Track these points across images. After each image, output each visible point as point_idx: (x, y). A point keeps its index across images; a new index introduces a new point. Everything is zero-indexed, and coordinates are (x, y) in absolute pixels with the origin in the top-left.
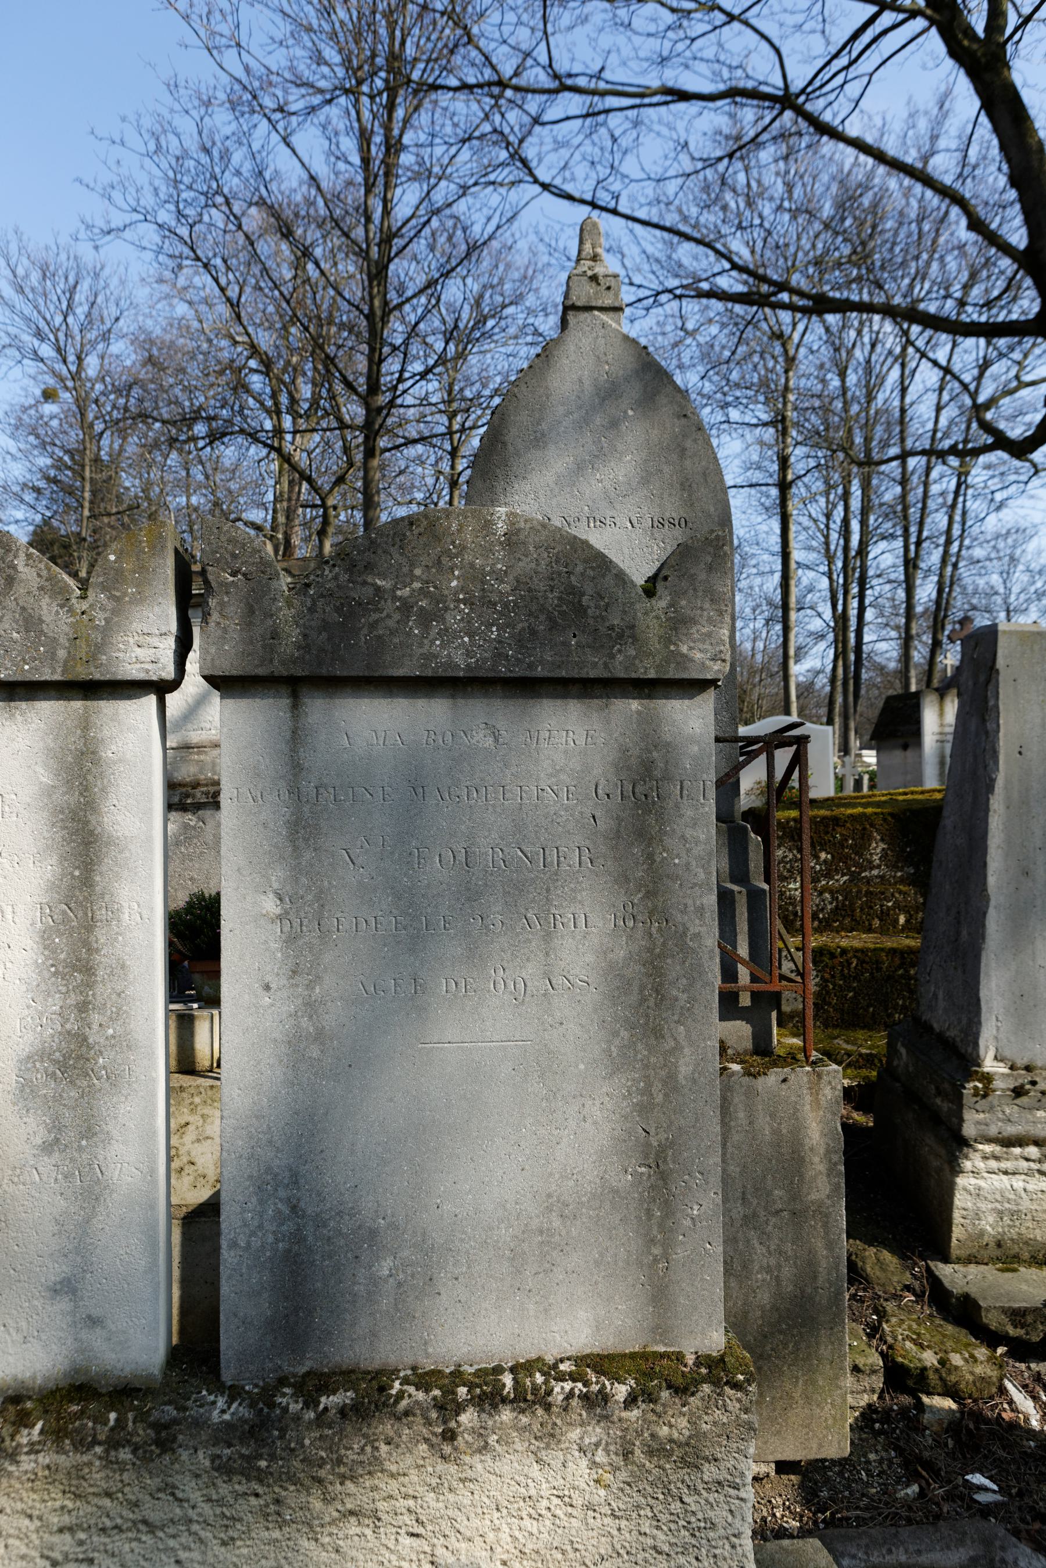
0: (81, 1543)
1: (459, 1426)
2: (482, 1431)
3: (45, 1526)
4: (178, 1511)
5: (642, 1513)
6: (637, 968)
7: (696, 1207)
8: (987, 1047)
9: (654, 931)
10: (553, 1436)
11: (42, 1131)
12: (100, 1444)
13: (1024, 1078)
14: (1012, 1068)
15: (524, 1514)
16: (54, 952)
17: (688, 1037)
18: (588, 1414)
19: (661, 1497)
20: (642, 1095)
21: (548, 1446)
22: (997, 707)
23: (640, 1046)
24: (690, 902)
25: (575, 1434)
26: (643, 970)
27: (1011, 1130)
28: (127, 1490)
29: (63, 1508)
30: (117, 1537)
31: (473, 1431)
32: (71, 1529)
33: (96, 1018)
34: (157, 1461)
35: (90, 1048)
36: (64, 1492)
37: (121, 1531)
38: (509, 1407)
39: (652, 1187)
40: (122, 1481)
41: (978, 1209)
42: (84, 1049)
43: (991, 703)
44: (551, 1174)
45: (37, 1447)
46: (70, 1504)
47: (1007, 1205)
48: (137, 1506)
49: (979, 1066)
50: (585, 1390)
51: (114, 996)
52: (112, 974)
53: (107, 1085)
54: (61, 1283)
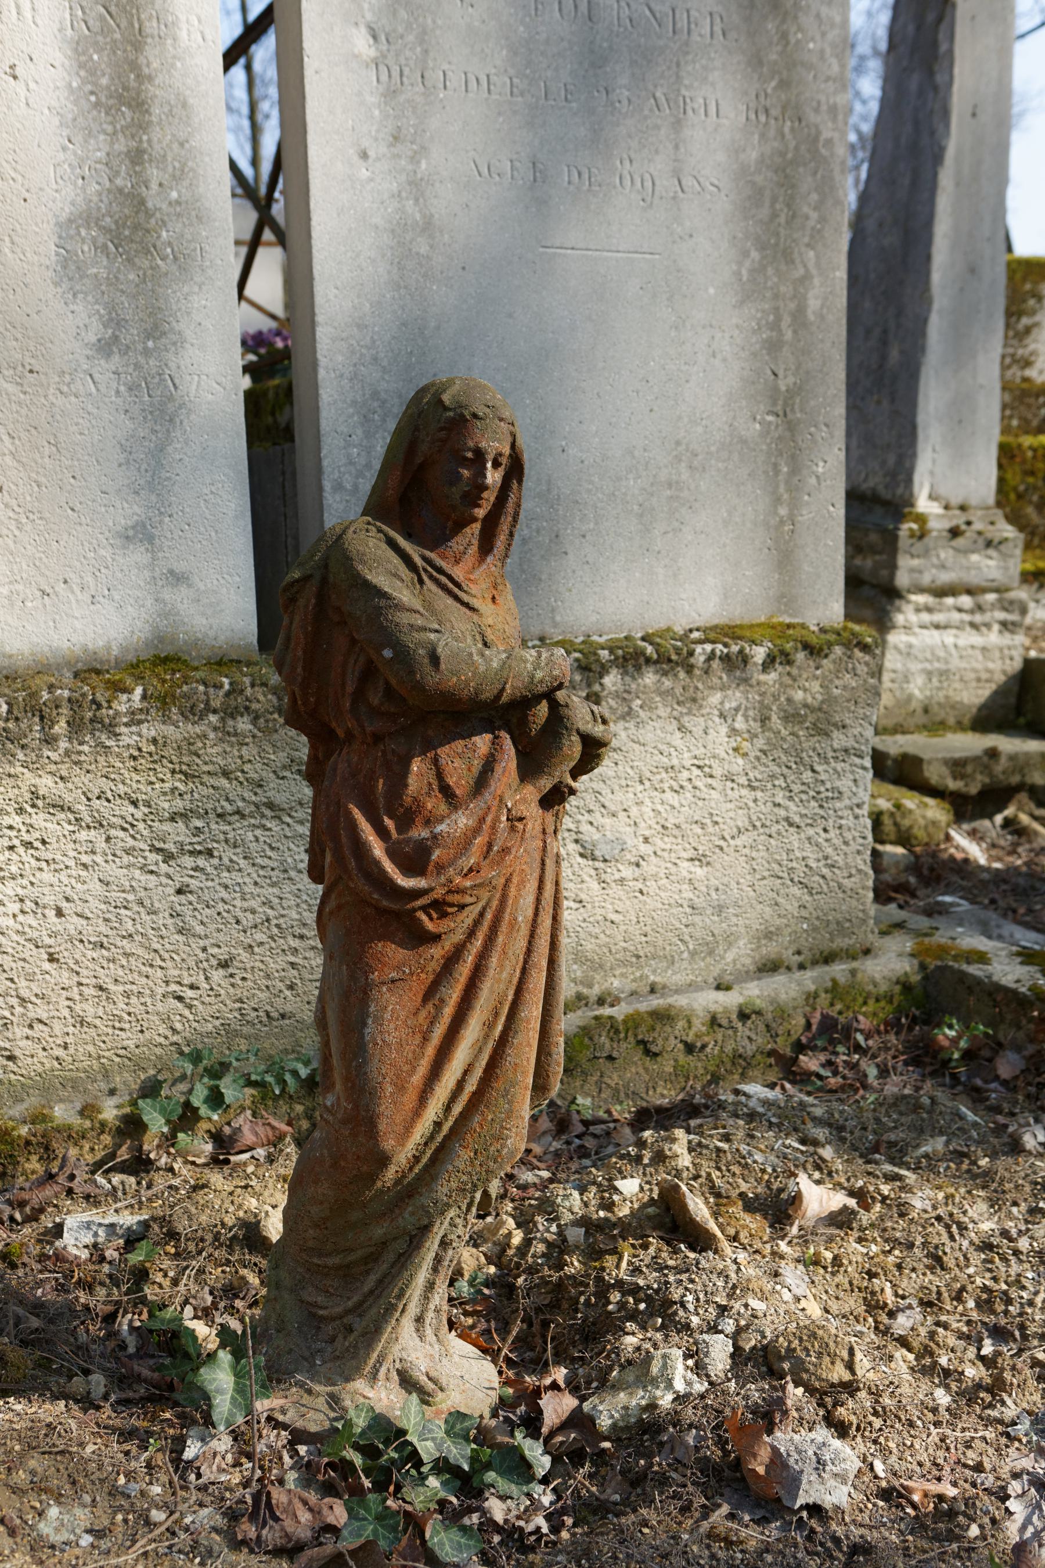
1: (603, 689)
2: (625, 695)
3: (153, 813)
5: (777, 783)
6: (769, 174)
7: (821, 464)
8: (921, 485)
9: (787, 130)
10: (694, 700)
11: (96, 325)
12: (215, 712)
13: (958, 519)
14: (947, 507)
15: (666, 786)
16: (92, 72)
17: (818, 265)
18: (728, 676)
19: (794, 766)
20: (772, 330)
22: (950, 52)
23: (770, 271)
24: (823, 99)
25: (715, 698)
26: (775, 178)
27: (945, 578)
28: (247, 767)
29: (174, 789)
31: (617, 695)
32: (184, 816)
33: (154, 174)
35: (149, 215)
36: (173, 772)
37: (243, 816)
38: (651, 669)
40: (241, 757)
41: (908, 670)
42: (142, 215)
43: (943, 48)
44: (680, 418)
45: (138, 717)
46: (181, 787)
47: (936, 665)
48: (261, 786)
49: (912, 505)
50: (725, 651)
51: (175, 146)
52: (170, 114)
53: (174, 268)
54: (133, 527)
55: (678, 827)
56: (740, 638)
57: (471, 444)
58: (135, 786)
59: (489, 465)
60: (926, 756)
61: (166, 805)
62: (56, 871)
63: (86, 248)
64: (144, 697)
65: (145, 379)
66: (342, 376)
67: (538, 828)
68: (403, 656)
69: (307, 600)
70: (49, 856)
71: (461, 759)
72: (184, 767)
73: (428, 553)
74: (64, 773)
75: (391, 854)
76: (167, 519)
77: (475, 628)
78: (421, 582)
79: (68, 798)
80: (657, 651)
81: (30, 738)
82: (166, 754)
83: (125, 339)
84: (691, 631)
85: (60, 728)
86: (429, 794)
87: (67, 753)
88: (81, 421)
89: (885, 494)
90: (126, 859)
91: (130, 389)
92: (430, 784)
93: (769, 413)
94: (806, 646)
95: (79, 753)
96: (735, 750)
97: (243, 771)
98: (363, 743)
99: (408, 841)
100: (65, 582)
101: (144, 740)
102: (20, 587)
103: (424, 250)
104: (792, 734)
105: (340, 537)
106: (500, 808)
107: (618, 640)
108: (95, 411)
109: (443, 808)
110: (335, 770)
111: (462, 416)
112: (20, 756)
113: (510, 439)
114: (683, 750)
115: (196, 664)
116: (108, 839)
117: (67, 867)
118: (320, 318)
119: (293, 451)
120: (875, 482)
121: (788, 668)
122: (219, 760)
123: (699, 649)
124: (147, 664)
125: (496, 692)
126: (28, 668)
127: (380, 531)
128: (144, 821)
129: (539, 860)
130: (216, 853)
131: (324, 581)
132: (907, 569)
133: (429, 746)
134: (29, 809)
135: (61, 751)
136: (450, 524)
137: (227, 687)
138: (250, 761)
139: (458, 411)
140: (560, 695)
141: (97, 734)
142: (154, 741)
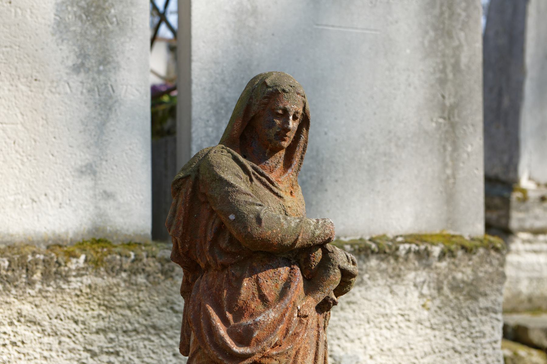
0: (111, 340)
4: (175, 319)
11: (72, 57)
12: (125, 271)
15: (383, 325)
18: (419, 263)
21: (396, 283)
23: (440, 42)
25: (411, 275)
27: (538, 224)
28: (142, 304)
29: (99, 315)
30: (134, 338)
34: (163, 284)
36: (99, 305)
39: (447, 132)
40: (138, 298)
46: (104, 314)
48: (149, 315)
54: (86, 166)
55: (390, 350)
56: (426, 241)
57: (281, 106)
58: (77, 312)
59: (291, 118)
60: (531, 325)
61: (94, 324)
62: (29, 360)
63: (70, 17)
64: (86, 261)
65: (97, 86)
66: (205, 89)
67: (315, 324)
68: (241, 218)
69: (187, 189)
70: (25, 351)
71: (273, 279)
72: (106, 303)
73: (255, 165)
74: (37, 303)
75: (230, 333)
76: (104, 163)
77: (280, 206)
78: (251, 180)
79: (39, 317)
80: (378, 247)
81: (20, 281)
82: (95, 294)
83: (88, 64)
84: (397, 237)
85: (37, 276)
86: (252, 300)
87: (40, 291)
88: (61, 107)
89: (502, 177)
90: (70, 355)
91: (89, 91)
92: (253, 294)
93: (441, 117)
94: (463, 248)
95: (47, 291)
96: (424, 306)
97: (139, 307)
98: (215, 270)
99: (240, 326)
100: (46, 195)
101: (84, 286)
102: (20, 197)
103: (252, 24)
104: (457, 298)
105: (207, 154)
106: (293, 309)
107: (355, 240)
108: (69, 102)
109: (261, 307)
110: (198, 286)
111: (277, 90)
112: (14, 291)
113: (302, 105)
114: (393, 305)
115: (115, 244)
116: (60, 343)
117: (35, 358)
118: (194, 58)
119: (175, 141)
120: (497, 171)
121: (453, 260)
122: (126, 299)
123: (402, 247)
124: (88, 243)
125: (293, 240)
126: (22, 242)
127: (229, 152)
128: (81, 333)
129: (315, 342)
130: (121, 354)
131: (197, 178)
132: (516, 219)
133: (253, 272)
134: (16, 323)
135: (37, 290)
136: (268, 150)
137: (133, 257)
138: (143, 301)
139: (275, 88)
140: (329, 246)
141: (58, 281)
142: (90, 286)
